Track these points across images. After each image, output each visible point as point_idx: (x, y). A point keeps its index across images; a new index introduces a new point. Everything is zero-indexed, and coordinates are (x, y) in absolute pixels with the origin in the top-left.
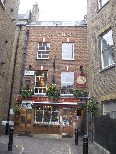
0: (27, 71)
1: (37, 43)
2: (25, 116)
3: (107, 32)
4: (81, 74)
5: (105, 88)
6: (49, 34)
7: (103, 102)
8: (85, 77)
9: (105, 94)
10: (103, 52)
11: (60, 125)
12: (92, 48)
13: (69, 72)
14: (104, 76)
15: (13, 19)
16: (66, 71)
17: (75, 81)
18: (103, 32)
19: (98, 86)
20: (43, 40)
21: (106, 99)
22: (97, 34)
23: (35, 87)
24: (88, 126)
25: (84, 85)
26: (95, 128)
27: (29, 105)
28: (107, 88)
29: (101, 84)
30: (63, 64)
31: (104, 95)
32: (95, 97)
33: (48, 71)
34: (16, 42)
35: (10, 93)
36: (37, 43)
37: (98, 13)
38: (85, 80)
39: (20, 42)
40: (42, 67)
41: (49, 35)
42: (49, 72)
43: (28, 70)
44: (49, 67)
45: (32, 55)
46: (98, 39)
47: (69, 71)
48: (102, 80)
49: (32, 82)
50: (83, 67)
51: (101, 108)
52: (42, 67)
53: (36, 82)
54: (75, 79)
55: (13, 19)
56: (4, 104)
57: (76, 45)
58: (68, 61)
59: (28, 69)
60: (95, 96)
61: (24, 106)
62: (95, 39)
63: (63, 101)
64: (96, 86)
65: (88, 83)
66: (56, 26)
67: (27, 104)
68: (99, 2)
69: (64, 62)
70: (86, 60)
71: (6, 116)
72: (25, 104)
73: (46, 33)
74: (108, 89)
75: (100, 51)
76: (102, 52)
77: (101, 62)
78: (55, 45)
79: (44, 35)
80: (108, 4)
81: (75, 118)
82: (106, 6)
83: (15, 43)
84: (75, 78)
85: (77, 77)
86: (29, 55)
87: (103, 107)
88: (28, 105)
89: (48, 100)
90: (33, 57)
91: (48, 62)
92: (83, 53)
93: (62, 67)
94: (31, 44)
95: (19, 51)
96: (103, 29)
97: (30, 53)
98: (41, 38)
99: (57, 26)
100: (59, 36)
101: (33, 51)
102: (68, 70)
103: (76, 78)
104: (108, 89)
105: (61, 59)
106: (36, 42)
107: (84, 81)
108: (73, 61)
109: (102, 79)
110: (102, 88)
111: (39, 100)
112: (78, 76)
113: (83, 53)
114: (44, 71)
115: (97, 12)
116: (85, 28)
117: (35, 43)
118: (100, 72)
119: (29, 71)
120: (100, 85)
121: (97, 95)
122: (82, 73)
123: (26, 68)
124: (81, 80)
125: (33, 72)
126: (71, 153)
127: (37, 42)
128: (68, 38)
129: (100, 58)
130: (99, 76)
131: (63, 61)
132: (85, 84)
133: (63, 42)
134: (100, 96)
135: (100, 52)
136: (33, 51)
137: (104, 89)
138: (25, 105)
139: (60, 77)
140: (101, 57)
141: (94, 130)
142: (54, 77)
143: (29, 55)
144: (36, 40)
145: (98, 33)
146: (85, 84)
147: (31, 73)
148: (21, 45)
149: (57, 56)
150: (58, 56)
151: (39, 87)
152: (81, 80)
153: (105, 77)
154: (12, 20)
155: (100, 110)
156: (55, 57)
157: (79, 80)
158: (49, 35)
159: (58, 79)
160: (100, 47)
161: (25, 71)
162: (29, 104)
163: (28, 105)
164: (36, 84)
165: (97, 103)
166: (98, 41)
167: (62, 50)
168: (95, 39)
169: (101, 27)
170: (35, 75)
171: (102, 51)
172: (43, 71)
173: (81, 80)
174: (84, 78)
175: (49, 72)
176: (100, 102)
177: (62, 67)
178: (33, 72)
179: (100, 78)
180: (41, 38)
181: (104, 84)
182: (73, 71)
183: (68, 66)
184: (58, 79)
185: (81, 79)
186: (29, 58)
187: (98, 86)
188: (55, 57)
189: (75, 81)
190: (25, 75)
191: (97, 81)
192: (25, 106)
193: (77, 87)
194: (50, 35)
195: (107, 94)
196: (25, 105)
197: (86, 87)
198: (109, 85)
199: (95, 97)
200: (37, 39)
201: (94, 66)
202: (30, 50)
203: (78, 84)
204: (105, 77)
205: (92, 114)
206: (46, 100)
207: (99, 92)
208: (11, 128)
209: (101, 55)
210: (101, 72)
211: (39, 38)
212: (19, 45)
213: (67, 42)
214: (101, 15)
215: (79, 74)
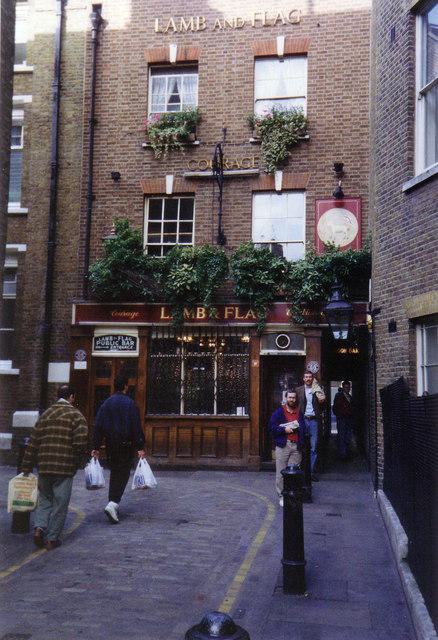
10: (424, 94)
13: (284, 196)
16: (273, 191)
20: (166, 51)
27: (123, 342)
33: (197, 198)
34: (52, 66)
35: (43, 295)
39: (68, 70)
40: (170, 180)
41: (195, 25)
46: (404, 28)
47: (284, 191)
48: (413, 226)
52: (170, 180)
53: (164, 242)
54: (312, 223)
56: (201, 315)
62: (393, 31)
71: (35, 388)
75: (412, 89)
77: (413, 145)
78: (222, 74)
79: (171, 28)
83: (46, 71)
84: (312, 220)
87: (413, 343)
88: (120, 343)
92: (349, 101)
95: (70, 110)
101: (127, 107)
102: (278, 187)
103: (316, 221)
111: (162, 317)
112: (325, 209)
113: (349, 101)
114: (179, 198)
128: (281, 34)
129: (409, 124)
133: (258, 58)
135: (412, 98)
140: (411, 119)
142: (220, 218)
148: (74, 83)
152: (339, 228)
156: (225, 130)
158: (195, 25)
159: (238, 229)
160: (412, 69)
166: (402, 39)
167: (256, 98)
168: (393, 31)
171: (418, 89)
172: (174, 198)
179: (406, 219)
180: (160, 43)
182: (302, 190)
183: (171, 173)
184: (238, 229)
188: (225, 130)
191: (392, 231)
195: (430, 290)
201: (384, 165)
204: (423, 211)
205: (85, 443)
208: (24, 441)
209: (411, 110)
212: (66, 83)
213: (275, 57)
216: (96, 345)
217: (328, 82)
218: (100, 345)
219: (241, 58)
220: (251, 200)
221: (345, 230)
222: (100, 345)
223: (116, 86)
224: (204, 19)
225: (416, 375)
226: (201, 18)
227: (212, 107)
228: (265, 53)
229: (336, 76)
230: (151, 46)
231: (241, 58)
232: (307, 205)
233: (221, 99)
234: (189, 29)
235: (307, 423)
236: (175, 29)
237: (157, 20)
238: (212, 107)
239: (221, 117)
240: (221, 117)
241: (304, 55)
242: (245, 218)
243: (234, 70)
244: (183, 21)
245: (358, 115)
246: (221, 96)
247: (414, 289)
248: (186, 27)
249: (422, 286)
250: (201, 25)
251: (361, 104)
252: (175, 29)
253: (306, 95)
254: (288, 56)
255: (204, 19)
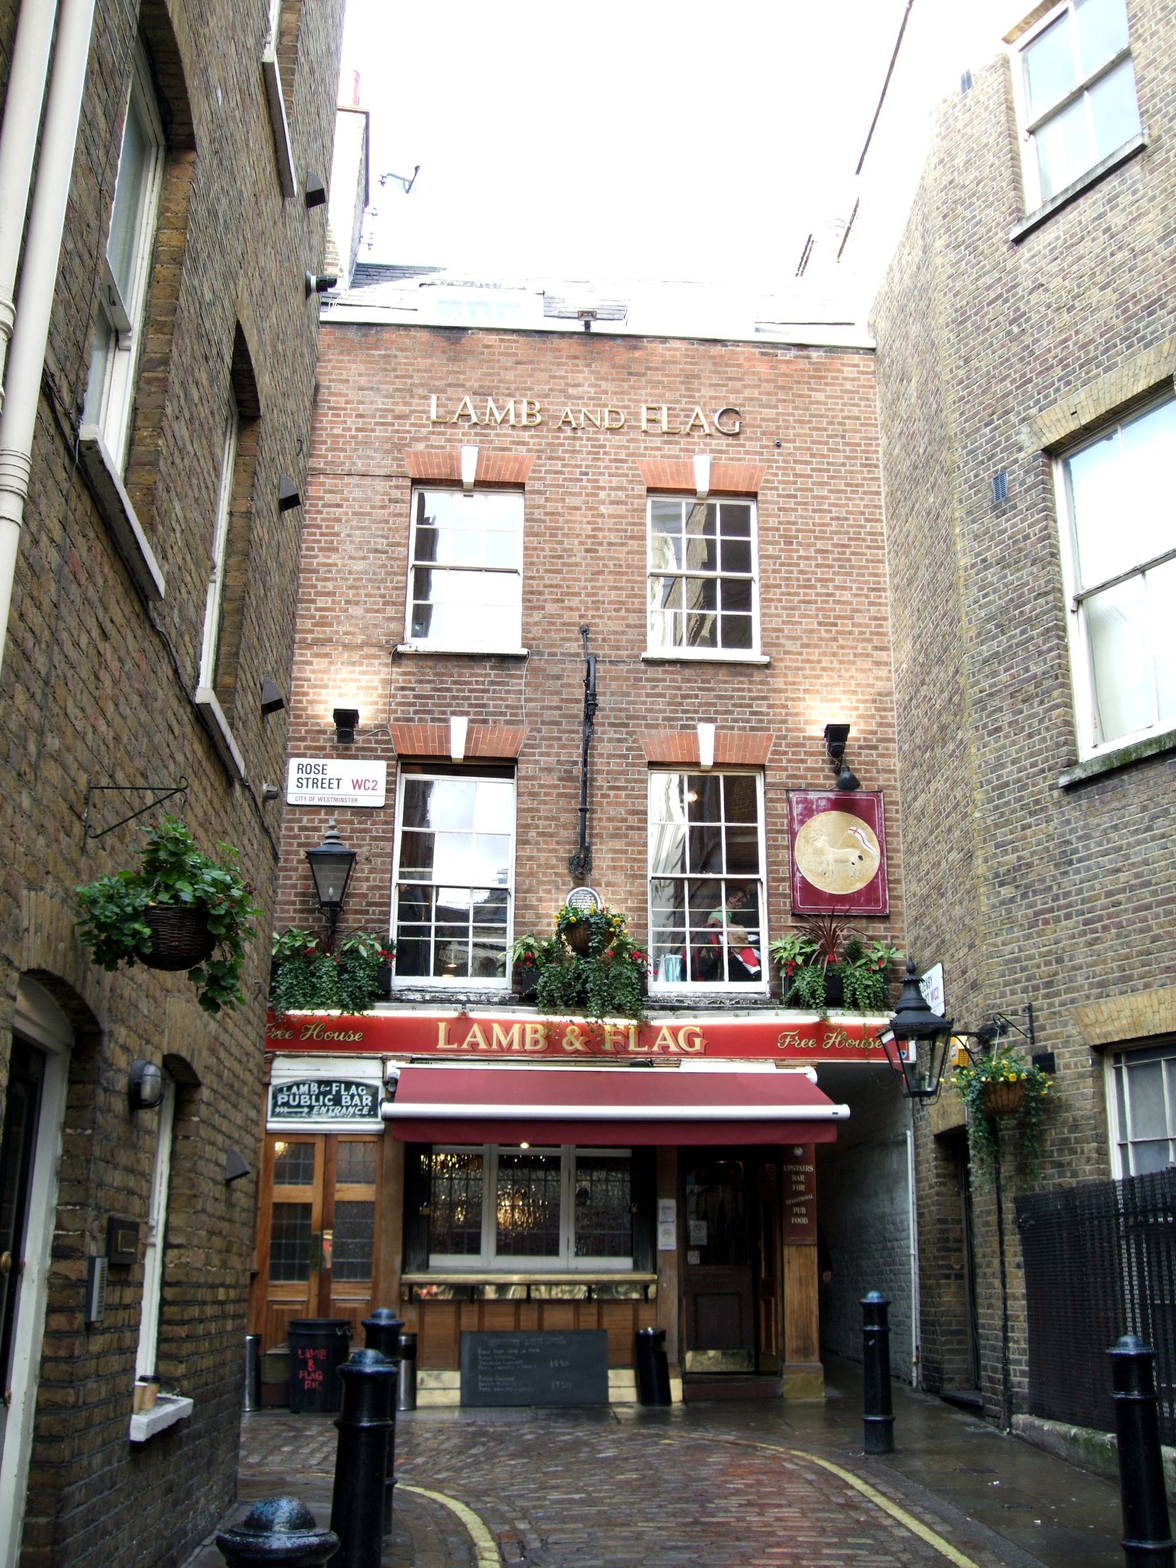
0: (313, 761)
1: (396, 494)
2: (307, 1208)
3: (1123, 427)
4: (831, 795)
5: (1119, 926)
6: (517, 409)
7: (1101, 1051)
8: (872, 825)
9: (1129, 978)
11: (656, 1282)
12: (964, 561)
14: (1105, 821)
15: (313, 280)
17: (780, 864)
18: (1086, 419)
19: (1051, 910)
21: (1135, 1024)
22: (1024, 437)
23: (394, 923)
24: (914, 1277)
25: (868, 903)
26: (1029, 1286)
27: (346, 1099)
28: (1150, 929)
29: (1080, 892)
30: (660, 704)
31: (1113, 989)
32: (1014, 1013)
36: (396, 494)
37: (1019, 240)
38: (874, 850)
41: (517, 416)
42: (533, 778)
43: (319, 752)
44: (525, 730)
45: (357, 611)
48: (1089, 857)
49: (362, 870)
50: (853, 733)
51: (1084, 1107)
55: (313, 280)
57: (772, 522)
58: (710, 671)
59: (323, 748)
60: (1020, 1000)
61: (295, 1110)
62: (999, 479)
63: (673, 1048)
64: (1021, 913)
65: (897, 881)
66: (578, 326)
67: (328, 1083)
68: (1022, 134)
69: (668, 678)
70: (877, 663)
72: (304, 1089)
73: (481, 393)
74: (1154, 939)
76: (1069, 604)
79: (465, 417)
80: (1134, 170)
81: (801, 1193)
82: (1113, 182)
85: (802, 822)
86: (322, 602)
88: (337, 1101)
89: (536, 1042)
90: (366, 627)
91: (519, 681)
92: (847, 596)
93: (656, 726)
94: (337, 499)
96: (1082, 394)
97: (330, 586)
98: (436, 440)
99: (588, 335)
100: (611, 430)
101: (359, 566)
104: (1154, 939)
105: (644, 655)
106: (389, 477)
107: (866, 860)
108: (758, 676)
109: (1087, 848)
110: (1095, 931)
111: (441, 1044)
112: (809, 812)
113: (847, 596)
115: (1017, 231)
116: (856, 359)
117: (381, 485)
118: (1064, 780)
119: (336, 767)
120: (1069, 905)
121: (1036, 988)
122: (851, 784)
123: (303, 739)
124: (832, 854)
125: (376, 770)
126: (503, 1560)
127: (400, 482)
128: (703, 452)
130: (1048, 820)
131: (658, 672)
132: (871, 891)
134: (1073, 1001)
136: (359, 566)
137: (1109, 938)
138: (305, 1100)
139: (633, 821)
141: (1019, 1308)
143: (322, 602)
144: (388, 465)
145: (1025, 429)
146: (872, 887)
147: (357, 784)
149: (605, 625)
150: (613, 626)
151: (433, 924)
153: (1115, 828)
154: (308, 290)
155: (1075, 1127)
156: (585, 631)
157: (819, 852)
158: (517, 416)
161: (294, 763)
162: (348, 1085)
163: (337, 1101)
164: (402, 896)
165: (1046, 1062)
169: (1058, 371)
170: (389, 807)
173: (832, 854)
174: (863, 832)
175: (533, 778)
176: (1075, 1054)
177: (647, 726)
178: (376, 770)
180: (436, 440)
181: (1109, 894)
184: (619, 844)
185: (833, 845)
186: (320, 633)
187: (1051, 910)
188: (585, 631)
189: (780, 864)
190: (291, 800)
192: (311, 1107)
193: (797, 916)
194: (525, 421)
196: (305, 1100)
197: (886, 918)
198: (1159, 904)
199: (1014, 1013)
200: (399, 447)
202: (334, 558)
203: (809, 891)
206: (516, 1046)
207: (1059, 960)
210: (1072, 788)
211: (421, 446)
214: (1054, 268)
215: (812, 796)
216: (275, 1105)
217: (802, 553)
218: (284, 1104)
219: (617, 489)
220: (645, 781)
221: (854, 858)
222: (284, 1104)
223: (338, 520)
224: (538, 406)
225: (1108, 1162)
226: (530, 403)
227: (556, 579)
228: (433, 473)
229: (819, 545)
230: (421, 446)
231: (617, 489)
232: (645, 797)
233: (576, 565)
234: (504, 421)
235: (94, 1361)
236: (474, 419)
237: (434, 398)
238: (556, 579)
239: (575, 602)
240: (575, 602)
241: (519, 486)
242: (633, 821)
243: (603, 509)
244: (491, 403)
245: (868, 626)
246: (578, 560)
247: (1101, 985)
248: (499, 418)
249: (1127, 979)
250: (530, 415)
251: (871, 604)
252: (474, 419)
253: (519, 565)
254: (483, 485)
255: (538, 406)
